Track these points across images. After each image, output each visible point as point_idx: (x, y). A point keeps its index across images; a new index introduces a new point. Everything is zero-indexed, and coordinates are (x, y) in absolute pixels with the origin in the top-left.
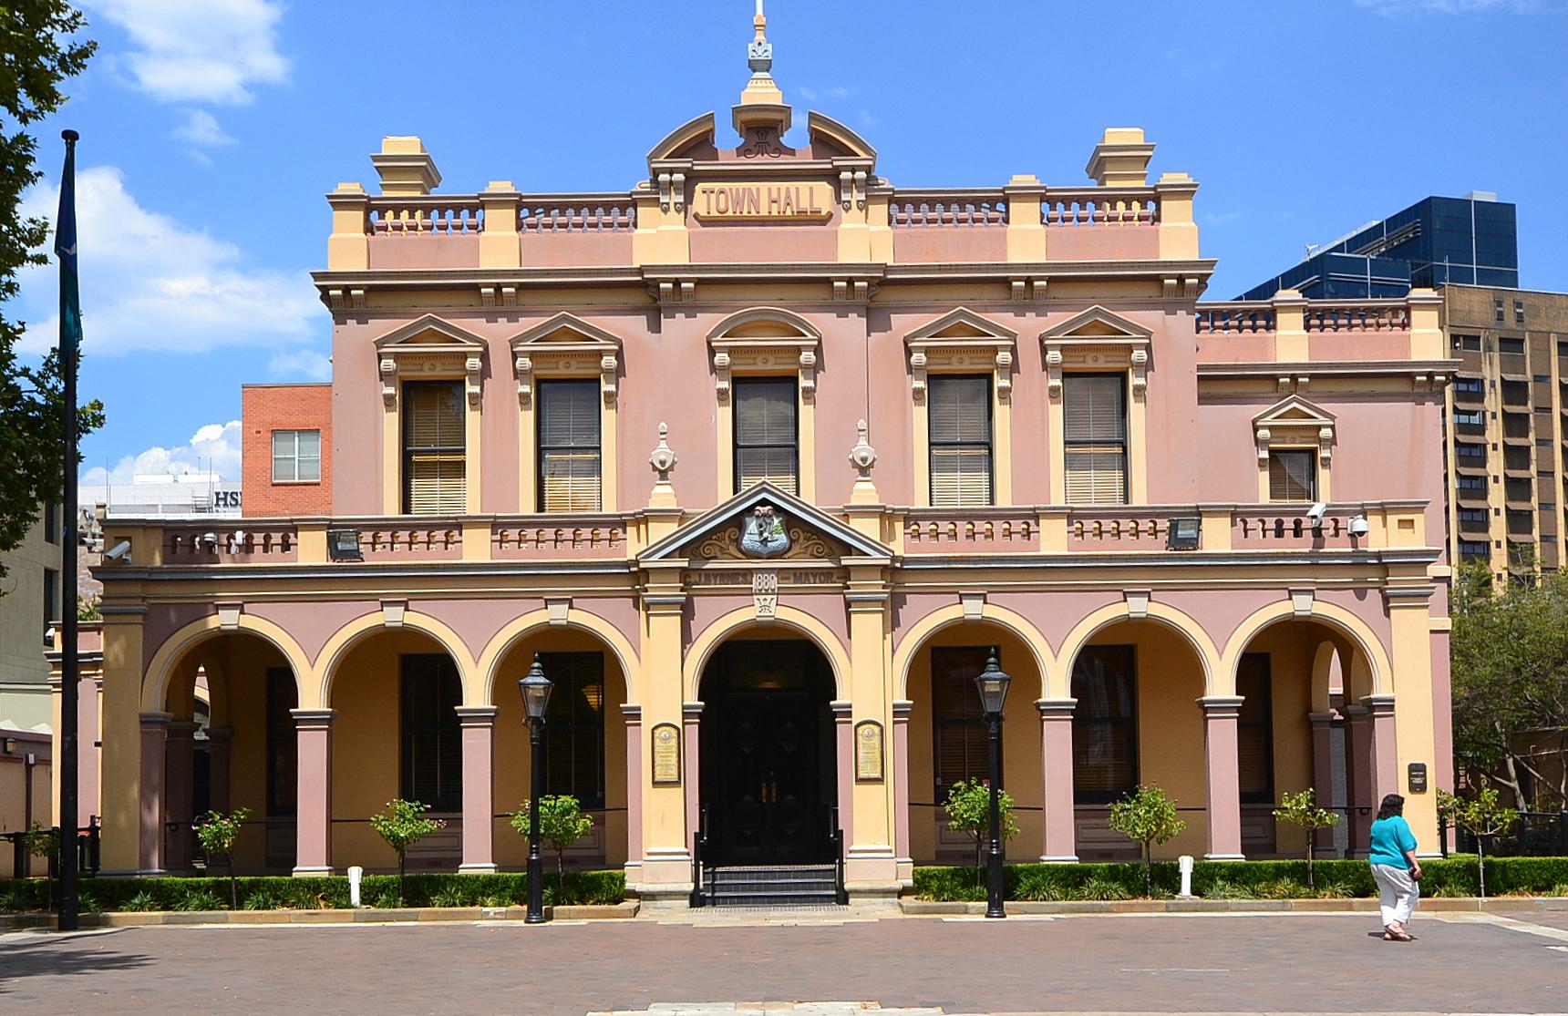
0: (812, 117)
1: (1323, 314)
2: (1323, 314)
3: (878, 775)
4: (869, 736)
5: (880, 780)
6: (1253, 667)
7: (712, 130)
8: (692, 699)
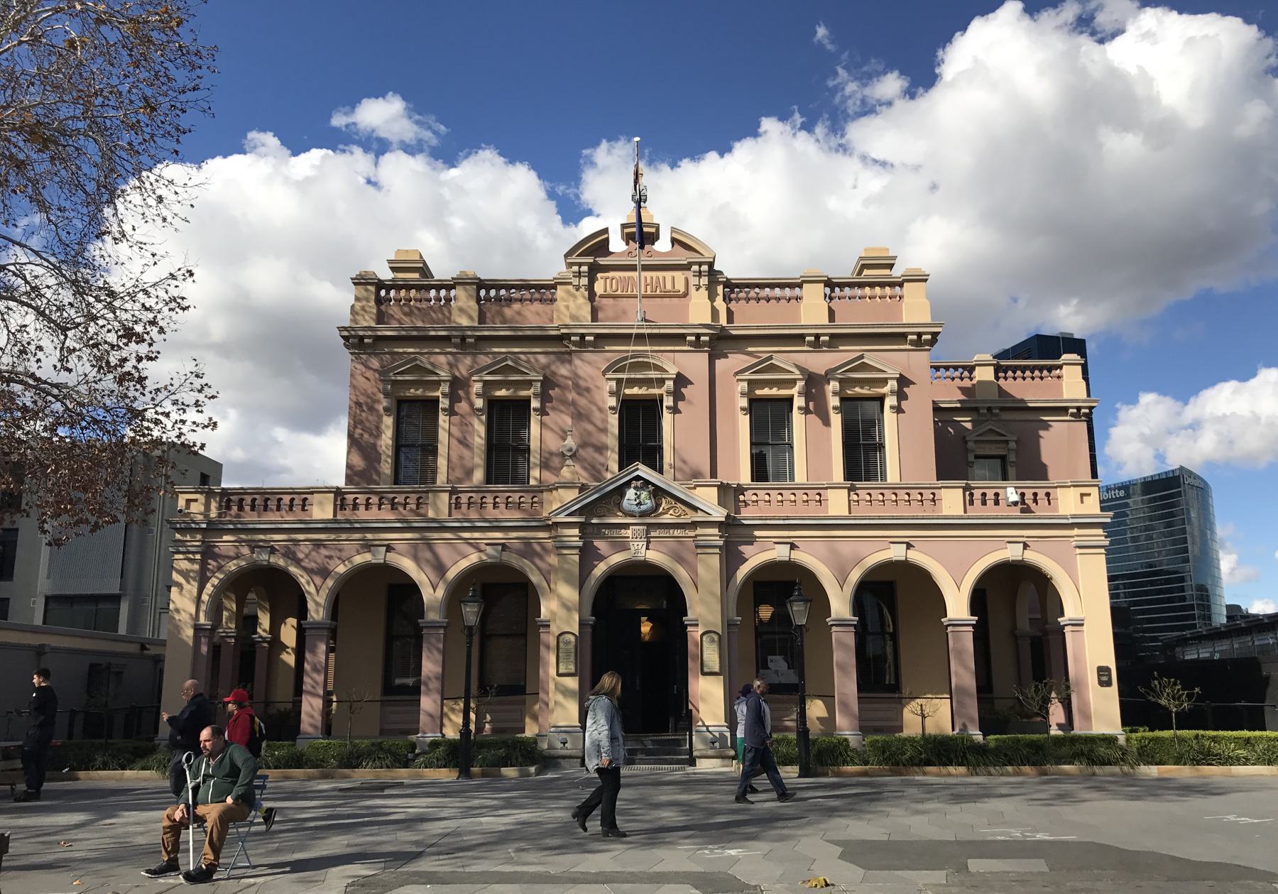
0: (673, 230)
1: (867, 472)
2: (867, 472)
6: (978, 600)
7: (607, 239)
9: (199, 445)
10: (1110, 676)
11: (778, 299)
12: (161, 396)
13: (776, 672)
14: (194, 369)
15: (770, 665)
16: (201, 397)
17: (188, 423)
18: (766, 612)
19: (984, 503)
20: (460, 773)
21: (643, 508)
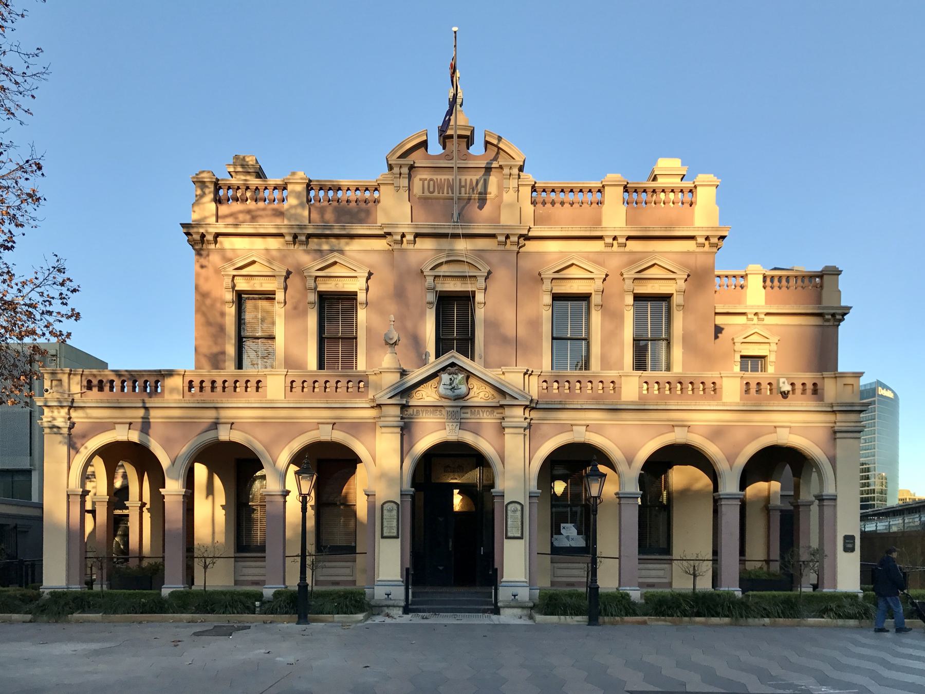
3: (519, 535)
4: (515, 511)
5: (521, 538)
8: (407, 486)
9: (65, 333)
10: (854, 543)
11: (553, 203)
12: (27, 289)
13: (568, 537)
14: (56, 265)
15: (562, 531)
16: (64, 290)
17: (54, 314)
18: (559, 487)
19: (213, 382)
20: (299, 618)
21: (457, 392)
